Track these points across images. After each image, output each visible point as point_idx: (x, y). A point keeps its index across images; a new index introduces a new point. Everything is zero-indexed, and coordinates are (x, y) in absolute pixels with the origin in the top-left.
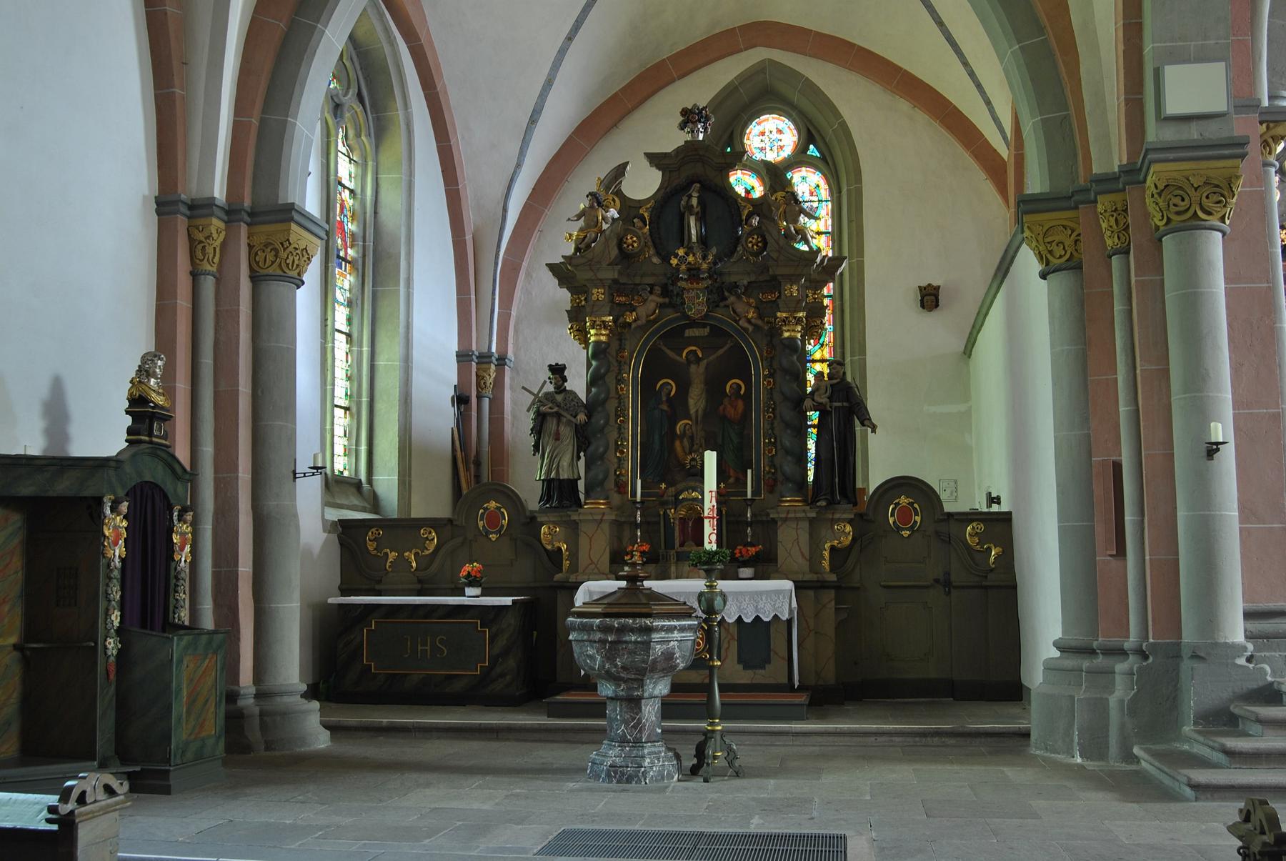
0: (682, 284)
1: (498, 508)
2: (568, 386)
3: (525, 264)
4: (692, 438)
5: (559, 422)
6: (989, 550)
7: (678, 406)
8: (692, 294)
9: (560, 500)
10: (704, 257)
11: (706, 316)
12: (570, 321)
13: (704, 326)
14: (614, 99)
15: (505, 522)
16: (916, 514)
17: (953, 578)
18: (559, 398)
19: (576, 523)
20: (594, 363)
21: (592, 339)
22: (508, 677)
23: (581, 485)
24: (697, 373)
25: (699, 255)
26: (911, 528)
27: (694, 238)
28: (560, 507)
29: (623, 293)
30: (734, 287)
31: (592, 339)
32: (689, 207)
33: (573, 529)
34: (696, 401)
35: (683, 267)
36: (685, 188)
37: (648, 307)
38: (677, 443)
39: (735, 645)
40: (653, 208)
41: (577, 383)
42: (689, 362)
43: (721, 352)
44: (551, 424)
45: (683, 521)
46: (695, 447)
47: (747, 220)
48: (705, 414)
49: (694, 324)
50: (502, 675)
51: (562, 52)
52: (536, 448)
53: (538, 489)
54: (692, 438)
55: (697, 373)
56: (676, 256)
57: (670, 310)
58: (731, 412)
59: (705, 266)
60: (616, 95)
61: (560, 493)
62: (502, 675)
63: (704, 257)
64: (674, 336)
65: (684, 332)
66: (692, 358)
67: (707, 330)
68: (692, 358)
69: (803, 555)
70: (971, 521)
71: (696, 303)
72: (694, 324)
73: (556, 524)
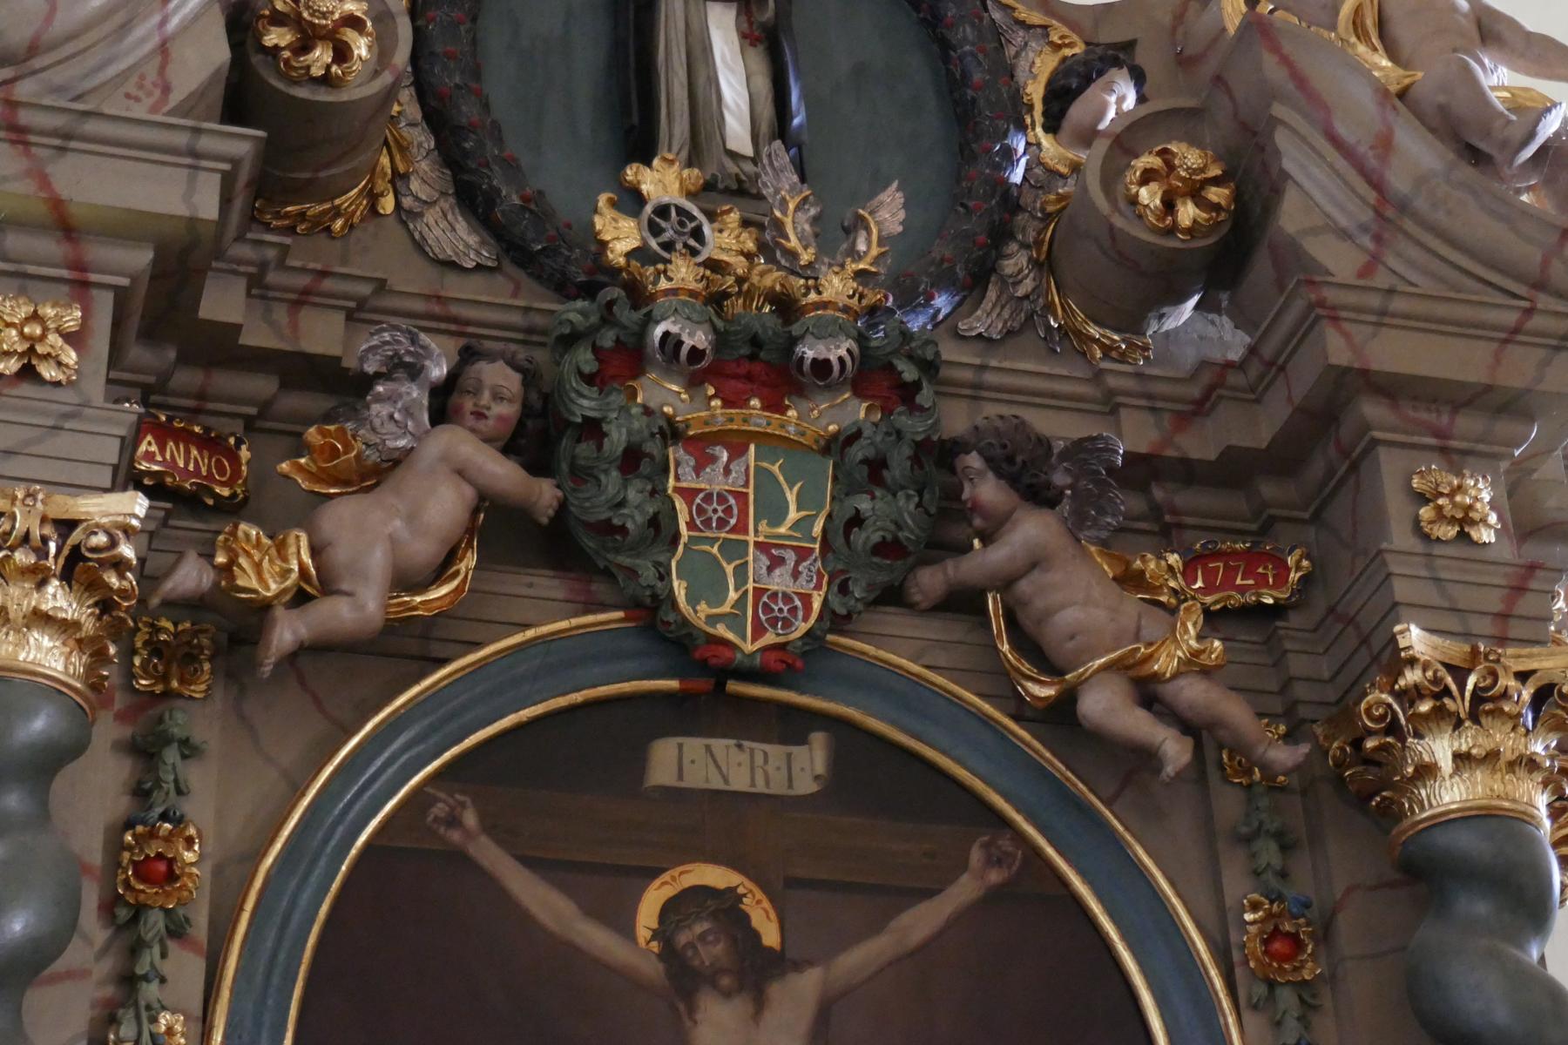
0: (664, 393)
8: (723, 475)
10: (836, 233)
13: (791, 726)
27: (737, 131)
37: (390, 526)
43: (921, 922)
47: (1061, 97)
49: (713, 689)
56: (631, 200)
57: (548, 585)
59: (836, 286)
63: (836, 233)
65: (639, 762)
66: (704, 943)
67: (805, 767)
68: (704, 943)
71: (752, 546)
72: (713, 689)
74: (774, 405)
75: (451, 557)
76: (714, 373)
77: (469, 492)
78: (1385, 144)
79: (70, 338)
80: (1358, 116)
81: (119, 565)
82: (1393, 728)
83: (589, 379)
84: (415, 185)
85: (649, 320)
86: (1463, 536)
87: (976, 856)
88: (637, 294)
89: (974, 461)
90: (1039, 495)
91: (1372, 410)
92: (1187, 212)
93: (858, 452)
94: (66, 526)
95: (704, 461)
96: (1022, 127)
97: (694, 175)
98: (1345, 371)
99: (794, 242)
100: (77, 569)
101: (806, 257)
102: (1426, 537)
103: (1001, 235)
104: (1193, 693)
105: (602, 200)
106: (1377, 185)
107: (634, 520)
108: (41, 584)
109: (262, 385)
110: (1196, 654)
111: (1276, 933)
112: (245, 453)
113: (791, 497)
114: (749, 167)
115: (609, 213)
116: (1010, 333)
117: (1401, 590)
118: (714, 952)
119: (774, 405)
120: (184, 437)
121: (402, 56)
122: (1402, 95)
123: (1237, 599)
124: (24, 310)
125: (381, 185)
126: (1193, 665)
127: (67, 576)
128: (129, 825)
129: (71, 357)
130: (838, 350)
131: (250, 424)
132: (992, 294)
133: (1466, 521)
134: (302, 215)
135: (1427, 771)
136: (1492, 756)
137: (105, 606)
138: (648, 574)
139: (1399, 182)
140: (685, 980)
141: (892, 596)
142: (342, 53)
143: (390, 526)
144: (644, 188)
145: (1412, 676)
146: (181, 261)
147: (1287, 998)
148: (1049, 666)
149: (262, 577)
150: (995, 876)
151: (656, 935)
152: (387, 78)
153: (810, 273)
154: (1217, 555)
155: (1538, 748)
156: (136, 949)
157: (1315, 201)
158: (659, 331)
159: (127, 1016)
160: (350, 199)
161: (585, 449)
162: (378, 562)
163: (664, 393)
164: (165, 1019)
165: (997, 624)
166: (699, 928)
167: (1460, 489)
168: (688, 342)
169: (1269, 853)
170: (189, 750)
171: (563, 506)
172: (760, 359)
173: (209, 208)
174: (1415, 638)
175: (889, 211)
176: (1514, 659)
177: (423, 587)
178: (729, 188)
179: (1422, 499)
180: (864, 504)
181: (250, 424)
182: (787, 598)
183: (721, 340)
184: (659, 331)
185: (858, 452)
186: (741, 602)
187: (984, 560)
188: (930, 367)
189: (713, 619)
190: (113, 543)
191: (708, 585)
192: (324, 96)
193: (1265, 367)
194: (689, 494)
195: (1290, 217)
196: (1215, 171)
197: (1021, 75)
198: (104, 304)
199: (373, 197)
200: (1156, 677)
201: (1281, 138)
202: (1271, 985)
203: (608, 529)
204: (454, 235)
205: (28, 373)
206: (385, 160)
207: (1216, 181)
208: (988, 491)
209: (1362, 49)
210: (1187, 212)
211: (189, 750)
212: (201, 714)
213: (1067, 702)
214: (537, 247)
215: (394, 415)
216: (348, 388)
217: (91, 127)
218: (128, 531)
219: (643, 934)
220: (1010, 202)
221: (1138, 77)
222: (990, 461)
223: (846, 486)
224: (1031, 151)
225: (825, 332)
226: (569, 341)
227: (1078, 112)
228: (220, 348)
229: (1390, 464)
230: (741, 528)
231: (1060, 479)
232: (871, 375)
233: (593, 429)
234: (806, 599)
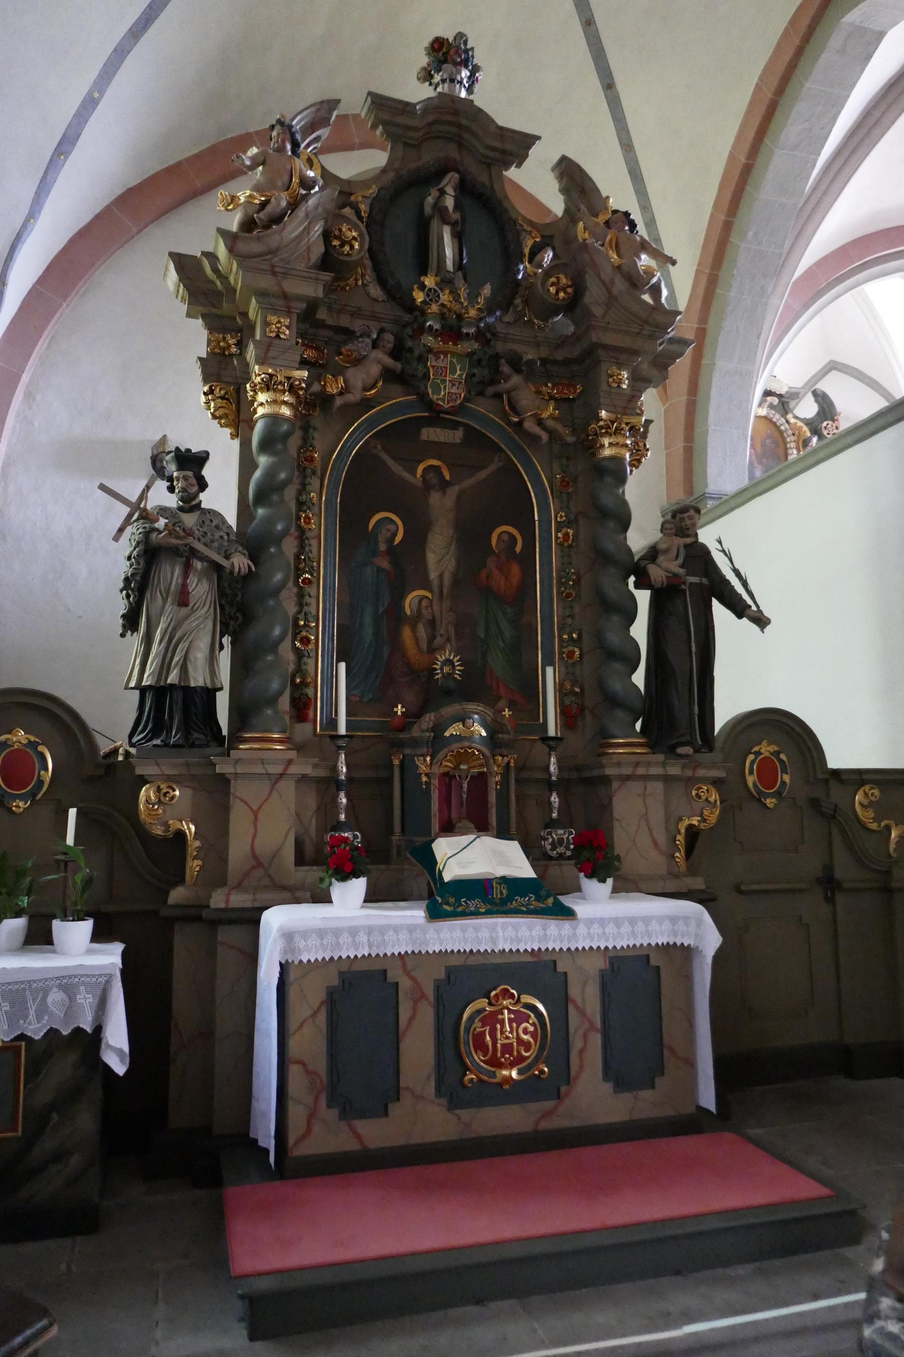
0: (429, 340)
1: (33, 745)
2: (207, 500)
3: (25, 378)
4: (432, 624)
5: (187, 569)
6: (888, 829)
7: (406, 565)
9: (186, 728)
10: (473, 297)
11: (460, 409)
12: (205, 381)
13: (455, 425)
14: (173, 172)
15: (48, 776)
16: (784, 771)
17: (838, 875)
18: (190, 520)
19: (224, 781)
20: (263, 461)
21: (261, 411)
22: (75, 1161)
23: (223, 701)
24: (442, 506)
25: (463, 292)
26: (778, 794)
27: (449, 264)
28: (188, 744)
29: (322, 337)
30: (516, 364)
31: (261, 411)
32: (440, 210)
33: (216, 793)
34: (440, 557)
35: (434, 308)
36: (432, 177)
37: (362, 377)
38: (407, 632)
39: (596, 1040)
40: (375, 201)
41: (222, 495)
42: (427, 487)
43: (482, 475)
44: (170, 574)
45: (447, 779)
46: (438, 641)
48: (456, 582)
50: (59, 1156)
51: (120, 53)
52: (131, 621)
53: (128, 707)
54: (432, 624)
55: (442, 506)
56: (422, 287)
57: (397, 388)
58: (499, 582)
59: (473, 313)
60: (179, 164)
61: (174, 710)
62: (59, 1156)
63: (473, 297)
64: (401, 436)
65: (418, 433)
66: (433, 479)
67: (457, 436)
68: (433, 479)
69: (655, 843)
70: (863, 783)
71: (448, 382)
72: (437, 416)
73: (172, 781)
74: (455, 344)
75: (376, 382)
76: (440, 335)
77: (381, 367)
78: (612, 282)
79: (288, 327)
80: (607, 272)
81: (302, 388)
82: (596, 434)
83: (411, 337)
84: (367, 277)
85: (426, 321)
86: (619, 386)
87: (496, 459)
88: (423, 313)
89: (503, 361)
90: (518, 371)
91: (601, 353)
92: (562, 295)
93: (475, 357)
94: (289, 378)
95: (438, 358)
96: (523, 263)
97: (438, 279)
98: (596, 343)
99: (462, 300)
100: (292, 389)
101: (465, 304)
102: (610, 386)
103: (514, 294)
104: (550, 423)
105: (415, 286)
106: (609, 291)
107: (420, 374)
108: (284, 393)
109: (328, 333)
110: (552, 414)
111: (564, 481)
112: (326, 351)
113: (458, 368)
114: (452, 275)
115: (416, 290)
116: (515, 321)
117: (602, 400)
118: (435, 481)
119: (455, 344)
120: (311, 347)
121: (366, 247)
122: (619, 267)
123: (564, 396)
124: (276, 320)
125: (359, 277)
126: (551, 417)
127: (290, 391)
128: (302, 448)
129: (287, 332)
130: (472, 330)
131: (326, 343)
132: (511, 310)
133: (620, 382)
134: (339, 286)
135: (602, 446)
136: (617, 444)
137: (298, 397)
138: (422, 388)
139: (615, 291)
140: (427, 487)
141: (481, 394)
142: (352, 247)
143: (362, 377)
144: (426, 283)
145: (601, 423)
146: (312, 306)
147: (565, 497)
148: (517, 414)
149: (332, 389)
150: (500, 464)
151: (422, 476)
152: (362, 254)
153: (466, 308)
154: (561, 384)
155: (629, 442)
156: (305, 477)
157: (594, 295)
158: (428, 324)
159: (304, 493)
160: (351, 281)
161: (408, 355)
162: (360, 384)
163: (429, 340)
164: (312, 494)
165: (506, 402)
166: (431, 475)
167: (620, 374)
168: (435, 327)
169: (564, 461)
170: (315, 429)
171: (403, 369)
172: (452, 330)
173: (320, 294)
174: (603, 414)
175: (487, 290)
176: (626, 419)
177: (369, 391)
178: (446, 282)
179: (611, 376)
180: (475, 371)
181: (326, 343)
182: (456, 394)
183: (443, 326)
184: (428, 324)
185: (475, 357)
186: (444, 395)
187: (503, 386)
188: (494, 335)
189: (438, 399)
190: (300, 384)
191: (437, 390)
192: (349, 259)
193: (576, 337)
194: (433, 367)
195: (587, 299)
196: (570, 283)
197: (523, 246)
198: (295, 317)
199: (356, 280)
200: (542, 419)
201: (587, 276)
202: (561, 493)
203: (413, 376)
204: (375, 291)
205: (278, 336)
206: (359, 270)
207: (570, 286)
208: (506, 369)
209: (610, 252)
210: (562, 295)
211: (315, 429)
212: (317, 419)
213: (520, 424)
214: (399, 297)
215: (362, 346)
216: (349, 334)
217: (292, 272)
218: (303, 380)
219: (418, 476)
220: (518, 283)
221: (554, 249)
222: (507, 362)
223: (471, 366)
224: (523, 270)
225: (469, 325)
226: (405, 326)
227: (538, 258)
228: (322, 325)
229: (604, 366)
230: (446, 376)
231: (524, 368)
232: (480, 336)
233: (411, 350)
234: (460, 395)
